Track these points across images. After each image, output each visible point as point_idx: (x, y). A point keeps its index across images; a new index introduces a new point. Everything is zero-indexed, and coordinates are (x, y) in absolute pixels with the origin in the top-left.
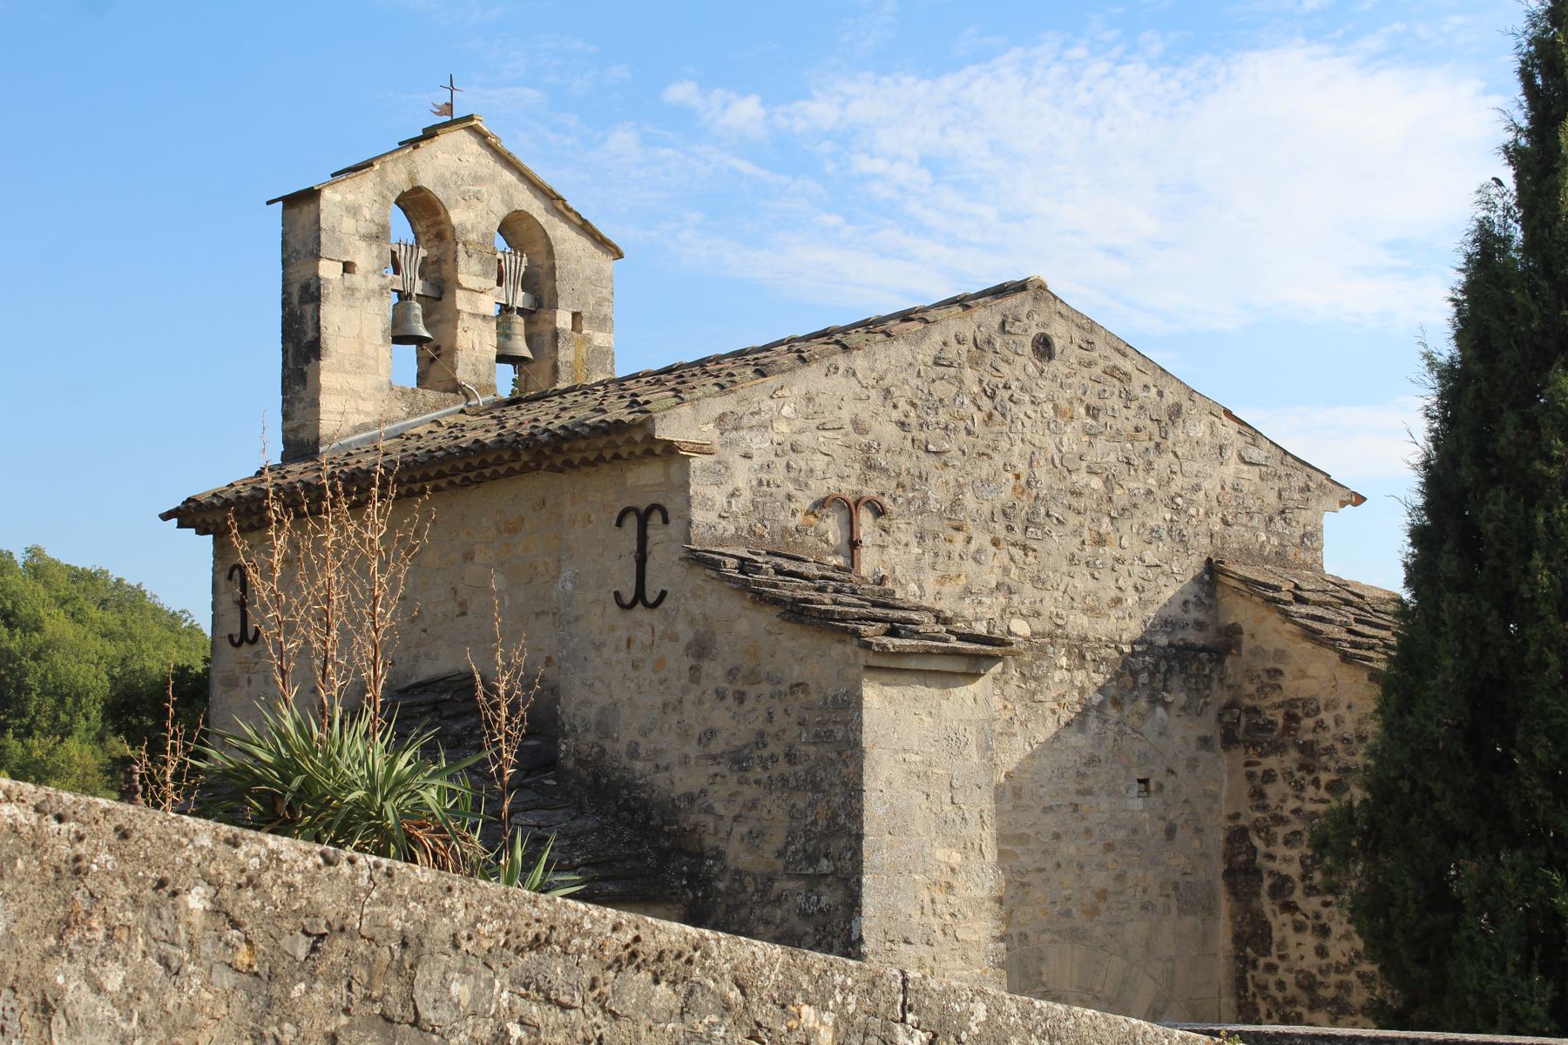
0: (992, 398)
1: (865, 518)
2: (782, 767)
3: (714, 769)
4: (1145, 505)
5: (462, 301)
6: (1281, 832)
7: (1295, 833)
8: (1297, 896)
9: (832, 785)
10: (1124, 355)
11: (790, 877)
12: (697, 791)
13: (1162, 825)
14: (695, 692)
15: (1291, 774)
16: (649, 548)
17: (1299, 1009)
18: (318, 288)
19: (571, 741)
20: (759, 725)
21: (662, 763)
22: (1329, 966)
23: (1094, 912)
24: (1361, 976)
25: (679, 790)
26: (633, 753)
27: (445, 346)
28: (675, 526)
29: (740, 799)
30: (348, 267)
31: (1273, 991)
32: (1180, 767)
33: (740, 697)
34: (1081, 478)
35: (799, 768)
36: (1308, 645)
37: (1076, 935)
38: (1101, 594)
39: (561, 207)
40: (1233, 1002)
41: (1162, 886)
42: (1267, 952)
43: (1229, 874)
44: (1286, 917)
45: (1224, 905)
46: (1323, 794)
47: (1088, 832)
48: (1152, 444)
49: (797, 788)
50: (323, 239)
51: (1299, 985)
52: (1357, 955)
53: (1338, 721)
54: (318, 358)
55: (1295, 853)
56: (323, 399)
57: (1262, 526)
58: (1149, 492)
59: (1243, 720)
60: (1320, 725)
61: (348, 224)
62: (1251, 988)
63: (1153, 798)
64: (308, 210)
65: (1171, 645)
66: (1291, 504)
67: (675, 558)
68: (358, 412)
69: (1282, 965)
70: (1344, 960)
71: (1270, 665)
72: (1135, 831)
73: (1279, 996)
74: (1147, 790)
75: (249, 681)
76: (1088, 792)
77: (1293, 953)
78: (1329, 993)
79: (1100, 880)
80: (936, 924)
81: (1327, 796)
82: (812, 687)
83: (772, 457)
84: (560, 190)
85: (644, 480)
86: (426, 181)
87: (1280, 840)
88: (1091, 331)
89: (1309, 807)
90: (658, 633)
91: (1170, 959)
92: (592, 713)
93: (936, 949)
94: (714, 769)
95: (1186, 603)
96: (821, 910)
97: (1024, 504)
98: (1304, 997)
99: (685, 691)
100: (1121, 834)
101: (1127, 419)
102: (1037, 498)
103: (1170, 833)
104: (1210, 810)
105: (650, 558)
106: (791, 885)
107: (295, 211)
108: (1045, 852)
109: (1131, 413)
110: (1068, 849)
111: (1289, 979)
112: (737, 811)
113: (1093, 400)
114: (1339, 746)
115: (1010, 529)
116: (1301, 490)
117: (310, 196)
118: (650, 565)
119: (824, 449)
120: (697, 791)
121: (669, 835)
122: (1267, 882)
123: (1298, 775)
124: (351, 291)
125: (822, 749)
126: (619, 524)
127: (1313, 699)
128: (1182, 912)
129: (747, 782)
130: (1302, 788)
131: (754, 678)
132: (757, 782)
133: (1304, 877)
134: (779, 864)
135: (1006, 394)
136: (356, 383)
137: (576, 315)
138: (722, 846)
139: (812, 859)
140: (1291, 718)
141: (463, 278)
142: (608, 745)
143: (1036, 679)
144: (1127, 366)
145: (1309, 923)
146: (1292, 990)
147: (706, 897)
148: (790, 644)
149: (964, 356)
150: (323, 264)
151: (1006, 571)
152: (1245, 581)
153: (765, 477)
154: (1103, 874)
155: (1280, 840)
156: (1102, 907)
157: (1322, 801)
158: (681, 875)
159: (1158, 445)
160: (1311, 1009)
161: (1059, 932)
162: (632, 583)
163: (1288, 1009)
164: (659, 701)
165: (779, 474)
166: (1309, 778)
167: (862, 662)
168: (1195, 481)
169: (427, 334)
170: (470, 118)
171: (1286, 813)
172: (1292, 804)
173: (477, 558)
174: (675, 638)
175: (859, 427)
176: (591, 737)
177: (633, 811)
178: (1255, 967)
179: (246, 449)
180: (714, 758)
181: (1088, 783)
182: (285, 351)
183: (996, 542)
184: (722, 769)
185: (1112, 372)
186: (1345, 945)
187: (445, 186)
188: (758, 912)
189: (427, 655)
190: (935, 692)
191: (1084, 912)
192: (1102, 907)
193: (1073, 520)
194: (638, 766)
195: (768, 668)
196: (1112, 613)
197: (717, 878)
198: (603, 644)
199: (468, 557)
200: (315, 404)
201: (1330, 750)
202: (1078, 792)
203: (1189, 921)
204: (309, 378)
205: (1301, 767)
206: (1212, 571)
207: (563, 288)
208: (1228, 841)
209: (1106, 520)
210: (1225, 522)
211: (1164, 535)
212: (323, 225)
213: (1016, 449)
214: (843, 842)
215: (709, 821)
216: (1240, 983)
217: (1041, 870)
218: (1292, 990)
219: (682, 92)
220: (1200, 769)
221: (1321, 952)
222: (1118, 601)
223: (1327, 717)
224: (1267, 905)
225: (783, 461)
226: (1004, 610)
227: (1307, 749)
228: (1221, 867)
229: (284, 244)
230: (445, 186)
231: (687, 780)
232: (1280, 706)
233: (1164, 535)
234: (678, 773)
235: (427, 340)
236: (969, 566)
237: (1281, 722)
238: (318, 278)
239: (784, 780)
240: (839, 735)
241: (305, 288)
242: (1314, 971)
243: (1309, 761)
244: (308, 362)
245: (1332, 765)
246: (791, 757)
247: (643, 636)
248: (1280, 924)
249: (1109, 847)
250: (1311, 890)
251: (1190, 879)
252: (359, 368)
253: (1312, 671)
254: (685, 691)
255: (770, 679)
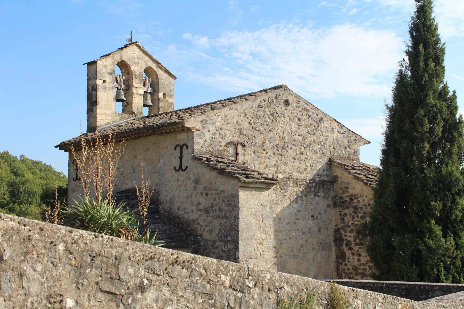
0: (273, 116)
1: (240, 147)
2: (218, 212)
3: (200, 213)
4: (313, 144)
5: (134, 90)
6: (348, 229)
7: (352, 230)
8: (353, 246)
9: (231, 217)
10: (308, 105)
11: (220, 241)
12: (195, 219)
13: (317, 227)
14: (195, 193)
15: (351, 214)
16: (183, 155)
17: (353, 275)
18: (96, 87)
19: (163, 206)
20: (212, 201)
21: (187, 211)
22: (361, 264)
23: (300, 250)
24: (369, 267)
25: (191, 219)
26: (179, 209)
27: (130, 102)
28: (190, 150)
29: (207, 221)
30: (104, 81)
31: (346, 271)
32: (322, 212)
33: (207, 194)
34: (296, 137)
35: (222, 213)
36: (356, 181)
37: (295, 256)
38: (302, 167)
39: (160, 66)
40: (336, 274)
41: (317, 243)
42: (345, 261)
43: (335, 240)
44: (350, 251)
45: (334, 248)
46: (359, 219)
47: (298, 229)
48: (315, 128)
49: (222, 218)
50: (98, 74)
51: (353, 269)
52: (368, 261)
53: (363, 200)
54: (96, 105)
55: (352, 235)
56: (97, 116)
57: (344, 149)
58: (314, 141)
59: (339, 200)
60: (359, 201)
61: (104, 70)
62: (341, 270)
63: (315, 220)
64: (93, 66)
65: (320, 181)
66: (351, 144)
67: (190, 158)
68: (107, 119)
69: (349, 264)
70: (365, 263)
71: (346, 186)
72: (310, 229)
73: (348, 272)
74: (314, 218)
75: (78, 190)
76: (298, 219)
77: (352, 261)
78: (361, 271)
79: (301, 242)
80: (258, 253)
81: (360, 220)
82: (226, 191)
83: (215, 131)
84: (160, 62)
85: (182, 138)
86: (125, 59)
87: (348, 231)
88: (299, 98)
89: (356, 223)
90: (185, 177)
91: (320, 263)
92: (168, 199)
93: (258, 260)
94: (200, 213)
95: (324, 170)
96: (228, 250)
97: (282, 144)
98: (354, 272)
99: (192, 193)
100: (307, 230)
101: (308, 122)
102: (285, 142)
103: (320, 230)
104: (330, 224)
105: (183, 158)
106: (220, 243)
107: (90, 67)
108: (287, 235)
109: (309, 120)
110: (293, 234)
111: (351, 268)
112: (206, 224)
113: (300, 117)
114: (363, 207)
115: (278, 150)
116: (354, 140)
117: (94, 63)
118: (183, 160)
119: (229, 129)
120: (195, 219)
121: (188, 230)
122: (345, 242)
123: (353, 214)
124: (105, 88)
125: (228, 208)
126: (175, 149)
127: (357, 195)
128: (323, 250)
129: (209, 216)
130: (354, 218)
131: (210, 189)
132: (211, 216)
133: (354, 241)
134: (217, 238)
135: (277, 115)
136: (106, 112)
137: (164, 94)
138: (202, 233)
139: (226, 237)
140: (351, 200)
141: (135, 84)
142: (172, 207)
143: (285, 189)
144: (308, 108)
145: (356, 253)
146: (351, 270)
147: (198, 246)
148: (220, 180)
149: (266, 105)
150: (98, 81)
151: (277, 161)
152: (339, 164)
153: (213, 136)
154: (302, 241)
155: (348, 231)
156: (302, 249)
157: (359, 221)
158: (192, 241)
159: (316, 128)
160: (356, 275)
161: (290, 256)
162: (179, 164)
163: (350, 275)
164: (186, 195)
165: (217, 136)
166: (356, 215)
167: (239, 185)
168: (326, 138)
169: (125, 99)
170: (136, 42)
171: (350, 224)
172: (351, 222)
173: (138, 158)
174: (190, 179)
175: (238, 123)
176: (168, 205)
177: (179, 224)
178: (342, 264)
179: (77, 129)
180: (200, 210)
181: (298, 217)
182: (88, 103)
183: (274, 154)
184: (202, 213)
185: (304, 109)
186: (365, 259)
187: (130, 60)
188: (211, 250)
189: (125, 183)
190: (258, 193)
191: (297, 250)
192: (302, 249)
193: (294, 148)
194: (180, 212)
195: (214, 187)
196: (304, 172)
197: (201, 241)
198: (171, 180)
199: (136, 157)
200: (95, 117)
201: (361, 208)
202: (296, 219)
203: (325, 253)
204: (94, 110)
205: (354, 212)
206: (331, 161)
207: (161, 87)
208: (335, 232)
209: (303, 148)
210: (334, 148)
211: (318, 152)
212: (98, 70)
213: (279, 129)
214: (234, 232)
215: (199, 227)
216: (338, 268)
217: (286, 239)
218: (351, 270)
219: (187, 36)
220: (327, 213)
221: (359, 260)
222: (306, 169)
223: (360, 199)
224: (345, 248)
225: (218, 132)
226: (276, 172)
227: (355, 208)
228: (333, 238)
229: (87, 75)
230: (130, 60)
231: (193, 216)
232: (348, 196)
233: (318, 152)
234: (191, 214)
235: (125, 101)
236: (267, 160)
237: (348, 201)
238: (96, 84)
239: (218, 216)
240: (233, 204)
241: (93, 87)
242: (357, 265)
243: (356, 211)
244: (93, 106)
245: (362, 212)
246: (220, 210)
247: (181, 178)
248: (348, 253)
249: (304, 233)
250: (356, 244)
251: (325, 241)
252: (107, 108)
253: (356, 187)
254: (192, 193)
255: (215, 190)
